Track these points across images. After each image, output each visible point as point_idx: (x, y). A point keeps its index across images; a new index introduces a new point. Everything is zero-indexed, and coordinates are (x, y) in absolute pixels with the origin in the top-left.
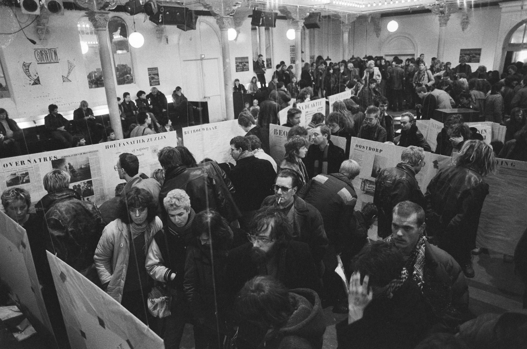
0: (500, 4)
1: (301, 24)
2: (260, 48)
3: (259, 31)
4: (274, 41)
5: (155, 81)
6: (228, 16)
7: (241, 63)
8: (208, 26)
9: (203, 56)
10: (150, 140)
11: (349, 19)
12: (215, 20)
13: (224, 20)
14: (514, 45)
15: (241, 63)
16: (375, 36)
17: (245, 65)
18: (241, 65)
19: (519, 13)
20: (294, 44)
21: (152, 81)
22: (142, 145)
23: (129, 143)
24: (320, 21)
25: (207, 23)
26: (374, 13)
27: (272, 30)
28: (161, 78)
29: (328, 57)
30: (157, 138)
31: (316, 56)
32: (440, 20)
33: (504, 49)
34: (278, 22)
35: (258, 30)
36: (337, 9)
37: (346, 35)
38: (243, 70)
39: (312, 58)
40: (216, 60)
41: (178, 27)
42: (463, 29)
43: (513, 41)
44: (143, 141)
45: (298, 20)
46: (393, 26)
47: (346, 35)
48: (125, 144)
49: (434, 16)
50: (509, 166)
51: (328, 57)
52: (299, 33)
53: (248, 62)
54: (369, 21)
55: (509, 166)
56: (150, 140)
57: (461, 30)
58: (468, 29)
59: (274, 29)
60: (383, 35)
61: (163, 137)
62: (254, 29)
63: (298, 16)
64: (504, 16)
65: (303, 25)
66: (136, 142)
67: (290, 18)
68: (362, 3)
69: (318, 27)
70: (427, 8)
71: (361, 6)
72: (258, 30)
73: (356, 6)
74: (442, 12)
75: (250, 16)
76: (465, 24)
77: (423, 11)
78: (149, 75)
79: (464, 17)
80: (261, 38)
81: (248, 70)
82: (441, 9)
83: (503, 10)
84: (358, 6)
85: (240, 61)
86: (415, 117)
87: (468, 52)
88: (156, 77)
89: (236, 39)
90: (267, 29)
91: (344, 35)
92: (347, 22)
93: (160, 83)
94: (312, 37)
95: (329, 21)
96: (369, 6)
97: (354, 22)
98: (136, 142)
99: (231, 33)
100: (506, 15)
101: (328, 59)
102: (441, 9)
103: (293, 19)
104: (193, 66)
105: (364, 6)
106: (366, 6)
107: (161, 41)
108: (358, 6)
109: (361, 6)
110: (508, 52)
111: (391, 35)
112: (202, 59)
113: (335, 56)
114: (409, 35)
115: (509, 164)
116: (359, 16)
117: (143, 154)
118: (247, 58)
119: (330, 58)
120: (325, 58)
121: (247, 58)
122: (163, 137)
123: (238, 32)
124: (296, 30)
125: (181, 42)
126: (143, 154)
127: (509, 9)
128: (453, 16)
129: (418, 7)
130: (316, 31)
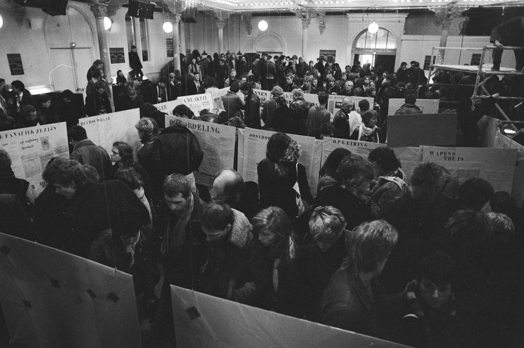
0: (347, 14)
1: (178, 18)
2: (135, 40)
3: (134, 22)
4: (150, 32)
5: (17, 69)
6: (104, 4)
7: (116, 54)
8: (78, 12)
9: (74, 45)
10: (39, 131)
11: (223, 16)
12: (89, 7)
13: (99, 8)
14: (359, 49)
15: (116, 54)
16: (247, 33)
17: (120, 57)
18: (116, 56)
19: (361, 23)
20: (172, 38)
21: (14, 69)
22: (31, 136)
23: (17, 134)
24: (196, 16)
25: (76, 9)
26: (247, 13)
27: (147, 22)
28: (26, 65)
29: (204, 51)
30: (47, 130)
31: (192, 49)
32: (303, 23)
33: (352, 51)
34: (156, 15)
35: (132, 21)
36: (212, 6)
37: (221, 32)
38: (118, 62)
39: (188, 51)
40: (88, 49)
41: (43, 10)
42: (321, 32)
43: (358, 46)
44: (32, 132)
45: (175, 13)
46: (263, 25)
47: (221, 32)
48: (13, 135)
49: (297, 19)
50: (364, 147)
51: (204, 51)
52: (177, 27)
53: (123, 54)
54: (242, 19)
55: (364, 147)
56: (39, 131)
57: (319, 33)
58: (325, 32)
59: (149, 21)
60: (254, 34)
61: (53, 128)
62: (127, 19)
63: (175, 9)
64: (351, 25)
65: (180, 19)
66: (24, 133)
67: (167, 11)
68: (235, 2)
69: (195, 22)
70: (292, 11)
71: (234, 5)
72: (132, 21)
73: (230, 4)
74: (304, 17)
75: (124, 6)
76: (322, 27)
77: (288, 14)
78: (320, 54)
79: (321, 23)
80: (136, 28)
81: (123, 61)
82: (303, 14)
83: (350, 19)
84: (232, 4)
85: (115, 52)
86: (356, 81)
87: (326, 53)
88: (19, 65)
89: (110, 29)
90: (142, 21)
91: (219, 31)
92: (221, 19)
93: (25, 72)
94: (187, 31)
95: (204, 16)
96: (242, 5)
97: (227, 19)
98: (24, 133)
99: (107, 22)
100: (352, 23)
101: (204, 53)
102: (303, 14)
103: (170, 13)
104: (64, 56)
105: (237, 5)
106: (239, 5)
107: (22, 24)
108: (232, 4)
109: (234, 5)
110: (355, 55)
111: (261, 34)
112: (72, 48)
113: (208, 50)
114: (278, 34)
115: (363, 145)
116: (233, 14)
117: (33, 146)
118: (122, 49)
119: (206, 52)
120: (201, 52)
121: (122, 49)
122: (53, 128)
123: (112, 22)
124: (174, 23)
125: (46, 28)
126: (33, 146)
127: (355, 19)
128: (313, 20)
129: (284, 10)
130: (191, 25)
